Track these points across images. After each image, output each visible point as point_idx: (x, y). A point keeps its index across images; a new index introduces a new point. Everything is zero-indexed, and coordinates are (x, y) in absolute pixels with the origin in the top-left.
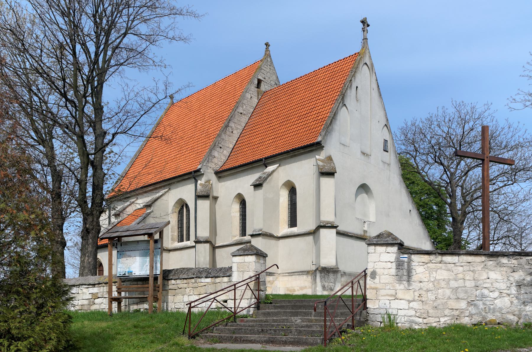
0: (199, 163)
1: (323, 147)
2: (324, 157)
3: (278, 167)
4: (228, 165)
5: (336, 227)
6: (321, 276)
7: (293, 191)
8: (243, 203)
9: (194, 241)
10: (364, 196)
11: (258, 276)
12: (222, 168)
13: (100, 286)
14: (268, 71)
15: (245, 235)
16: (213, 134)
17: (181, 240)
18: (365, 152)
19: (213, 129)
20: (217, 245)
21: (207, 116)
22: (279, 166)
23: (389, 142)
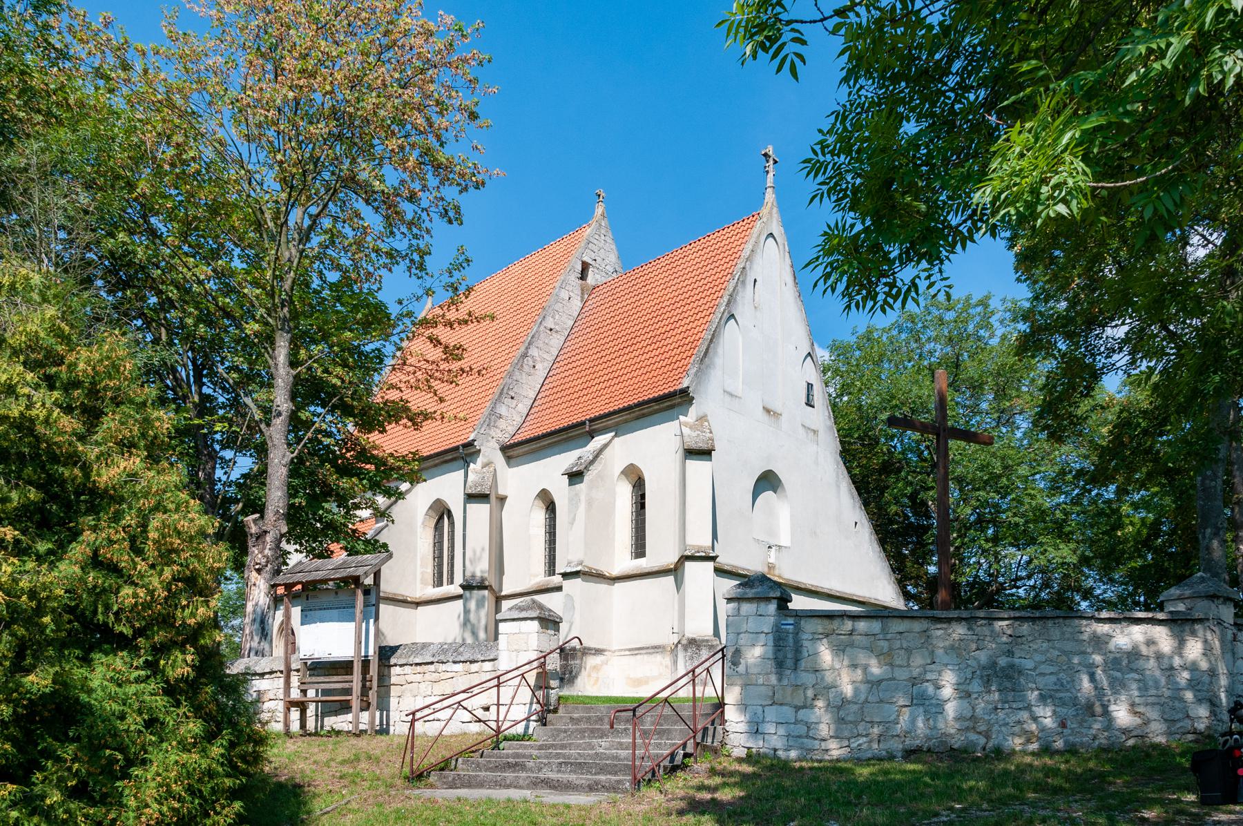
0: (471, 429)
1: (693, 398)
2: (695, 419)
3: (613, 438)
4: (526, 434)
5: (713, 559)
6: (685, 657)
7: (639, 485)
8: (551, 507)
9: (461, 586)
10: (768, 495)
11: (542, 660)
12: (517, 436)
13: (273, 676)
14: (601, 245)
15: (554, 574)
16: (499, 371)
17: (439, 583)
18: (769, 407)
19: (499, 360)
20: (503, 593)
21: (490, 335)
22: (616, 436)
23: (815, 387)
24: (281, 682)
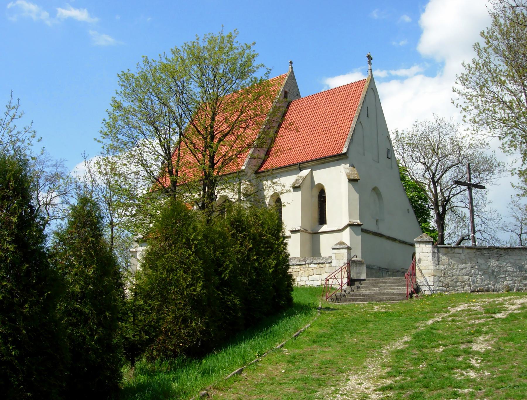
24: (442, 285)
